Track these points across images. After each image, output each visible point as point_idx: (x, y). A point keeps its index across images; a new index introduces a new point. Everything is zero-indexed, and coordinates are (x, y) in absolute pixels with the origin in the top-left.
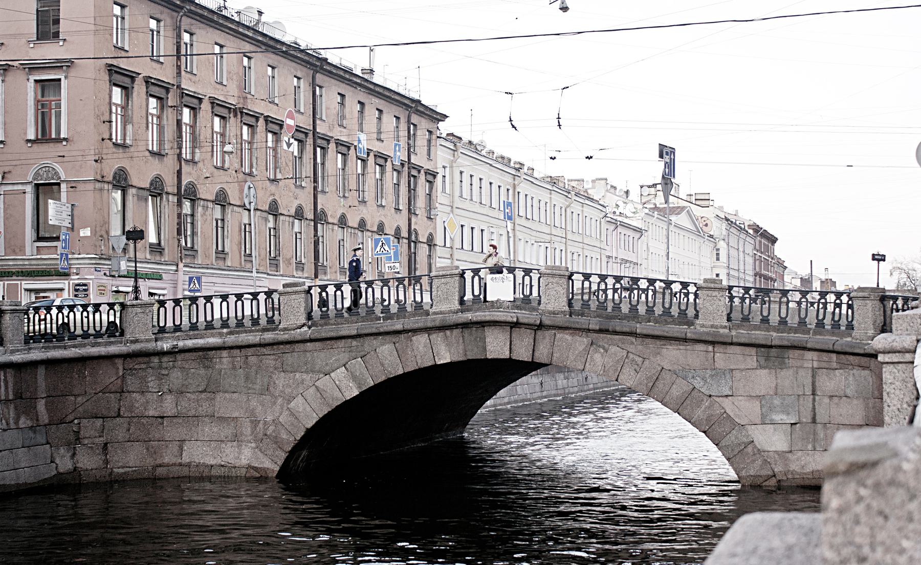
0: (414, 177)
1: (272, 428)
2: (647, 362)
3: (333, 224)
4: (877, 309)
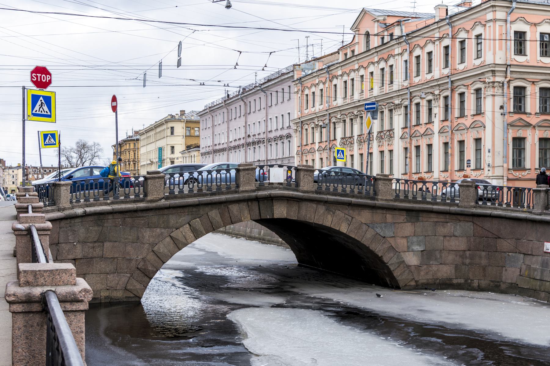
2: (354, 220)
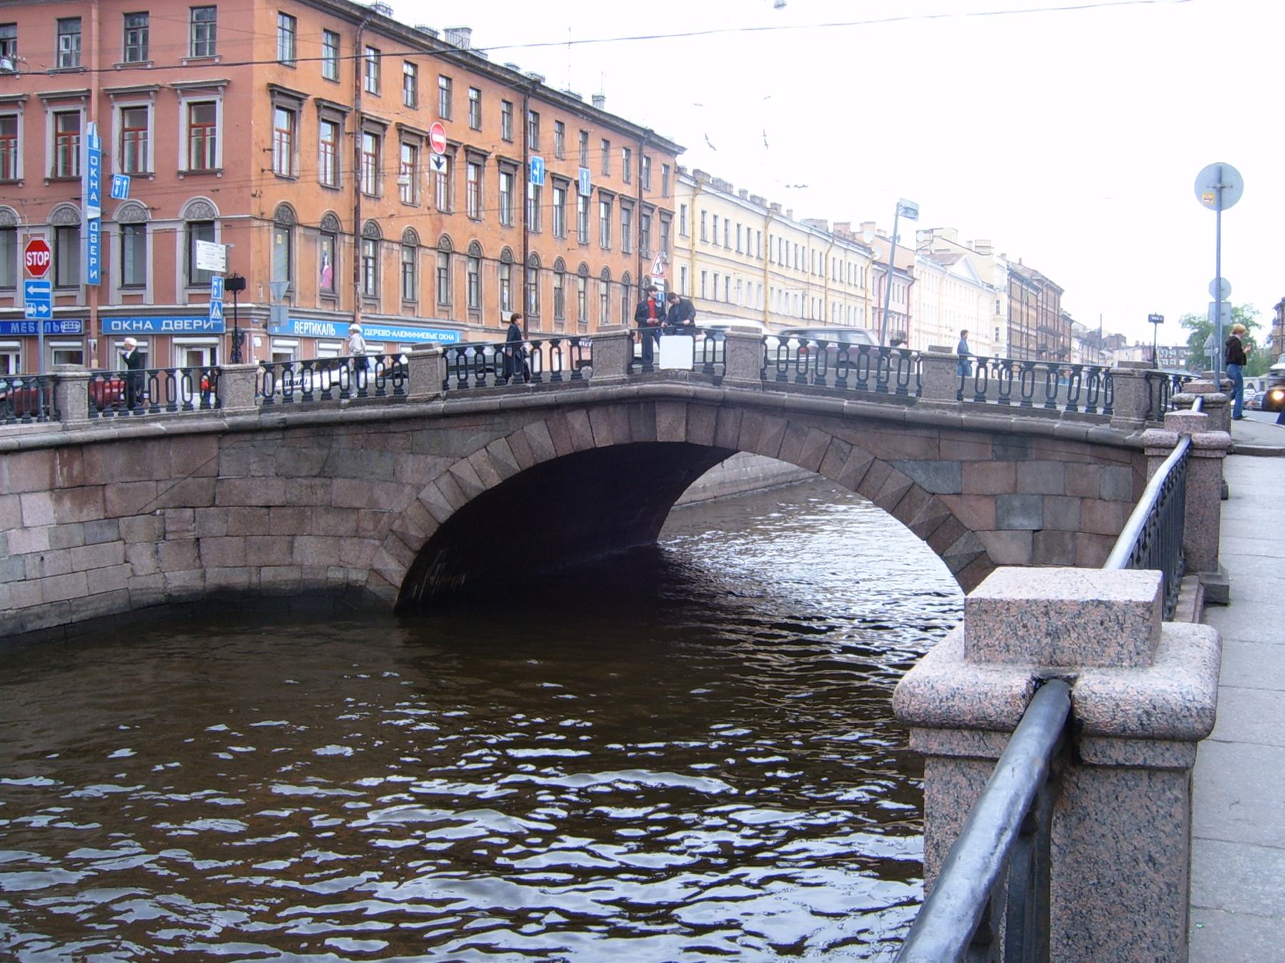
0: (647, 217)
1: (398, 522)
2: (855, 450)
3: (547, 269)
4: (1141, 390)
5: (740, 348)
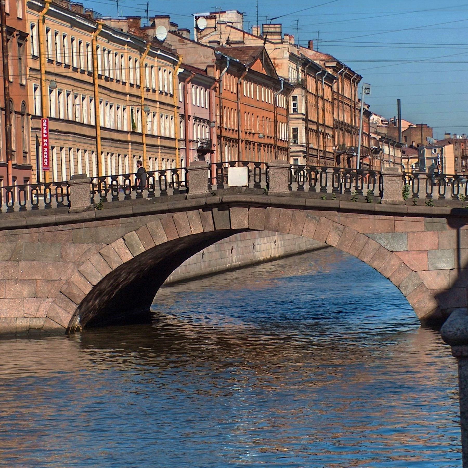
1: (65, 287)
5: (277, 173)
